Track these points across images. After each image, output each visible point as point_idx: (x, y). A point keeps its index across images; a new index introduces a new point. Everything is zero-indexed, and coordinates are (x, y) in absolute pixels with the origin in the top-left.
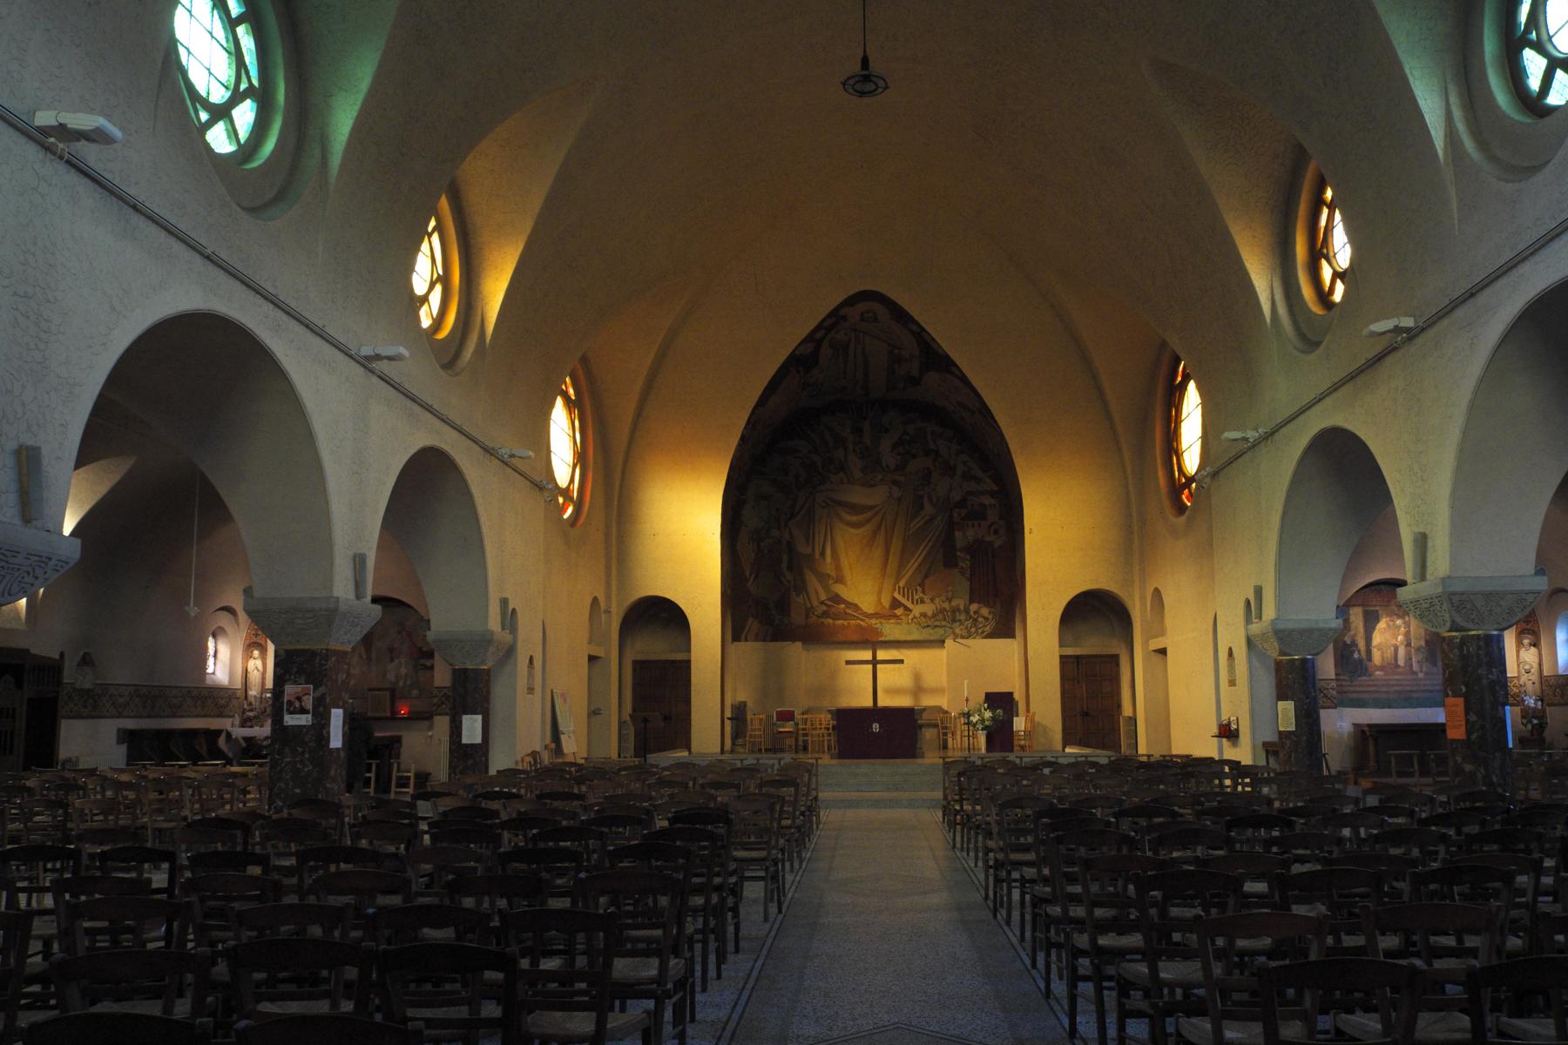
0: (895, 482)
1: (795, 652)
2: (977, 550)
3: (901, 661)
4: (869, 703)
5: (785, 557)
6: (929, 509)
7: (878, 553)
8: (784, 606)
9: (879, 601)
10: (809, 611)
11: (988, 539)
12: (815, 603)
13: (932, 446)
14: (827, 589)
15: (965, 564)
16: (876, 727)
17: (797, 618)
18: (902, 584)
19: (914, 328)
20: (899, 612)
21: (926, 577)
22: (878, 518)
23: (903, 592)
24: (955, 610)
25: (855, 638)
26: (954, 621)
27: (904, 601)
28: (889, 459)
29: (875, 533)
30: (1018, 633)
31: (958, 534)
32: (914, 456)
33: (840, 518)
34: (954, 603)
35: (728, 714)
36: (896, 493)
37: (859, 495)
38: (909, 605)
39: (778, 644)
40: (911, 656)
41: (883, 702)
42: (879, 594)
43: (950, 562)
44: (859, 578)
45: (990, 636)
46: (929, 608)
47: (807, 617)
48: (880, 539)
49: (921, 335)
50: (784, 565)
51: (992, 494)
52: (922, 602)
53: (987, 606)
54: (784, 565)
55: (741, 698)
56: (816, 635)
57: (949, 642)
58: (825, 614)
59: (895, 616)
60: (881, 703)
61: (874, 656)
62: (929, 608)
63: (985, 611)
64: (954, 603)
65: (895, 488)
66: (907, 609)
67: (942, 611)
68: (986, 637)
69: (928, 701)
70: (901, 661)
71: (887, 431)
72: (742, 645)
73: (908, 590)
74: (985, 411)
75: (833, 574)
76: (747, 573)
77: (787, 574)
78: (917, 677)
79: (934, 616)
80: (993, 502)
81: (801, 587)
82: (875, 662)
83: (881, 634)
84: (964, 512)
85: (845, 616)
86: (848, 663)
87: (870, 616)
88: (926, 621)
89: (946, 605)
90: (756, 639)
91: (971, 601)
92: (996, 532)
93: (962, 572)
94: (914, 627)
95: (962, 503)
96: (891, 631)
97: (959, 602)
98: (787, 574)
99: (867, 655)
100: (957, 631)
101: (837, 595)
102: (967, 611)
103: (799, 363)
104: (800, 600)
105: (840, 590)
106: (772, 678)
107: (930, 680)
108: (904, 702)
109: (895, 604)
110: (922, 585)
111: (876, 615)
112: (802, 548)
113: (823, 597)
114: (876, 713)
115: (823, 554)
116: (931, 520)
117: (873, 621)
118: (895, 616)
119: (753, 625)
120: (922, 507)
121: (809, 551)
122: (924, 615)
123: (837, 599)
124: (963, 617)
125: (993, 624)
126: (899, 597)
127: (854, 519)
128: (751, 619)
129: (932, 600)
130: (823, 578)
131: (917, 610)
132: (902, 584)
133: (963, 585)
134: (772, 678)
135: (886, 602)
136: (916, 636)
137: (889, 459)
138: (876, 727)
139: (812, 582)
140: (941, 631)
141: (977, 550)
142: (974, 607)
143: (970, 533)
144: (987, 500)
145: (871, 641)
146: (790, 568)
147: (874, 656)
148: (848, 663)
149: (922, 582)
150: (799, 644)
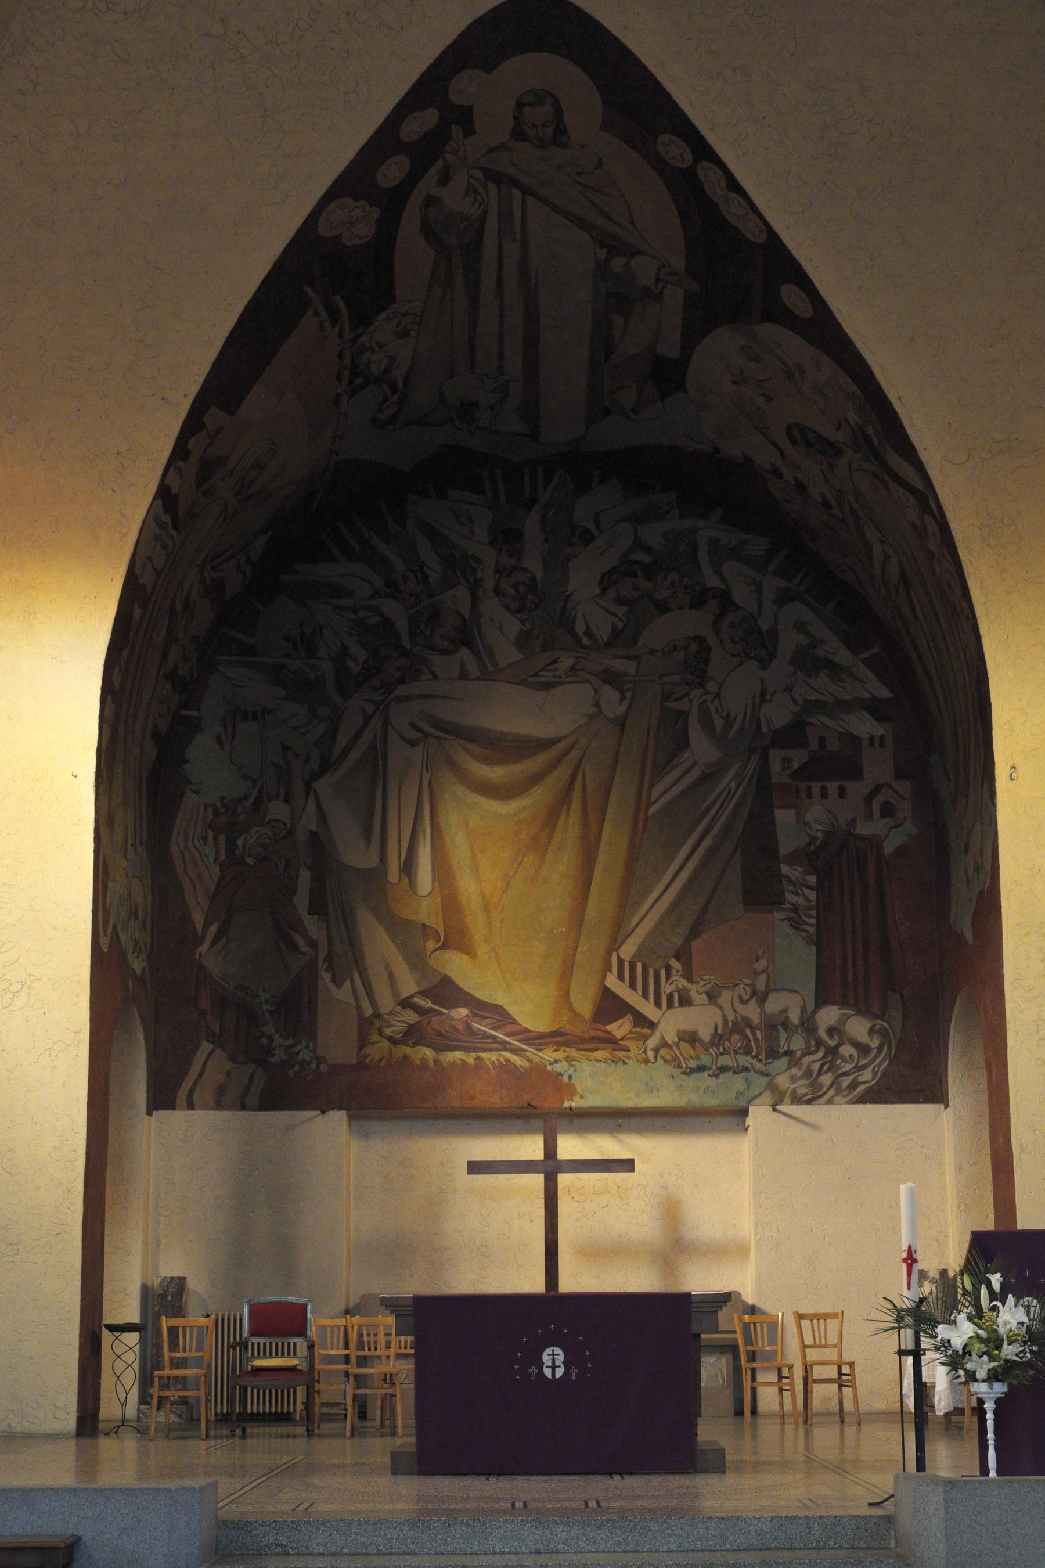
0: (610, 677)
1: (327, 1135)
2: (836, 859)
3: (627, 1165)
4: (534, 1283)
5: (305, 877)
6: (702, 749)
7: (561, 865)
8: (297, 1008)
9: (565, 998)
10: (367, 1026)
11: (863, 829)
12: (386, 1003)
13: (712, 581)
14: (418, 962)
15: (802, 890)
16: (553, 1361)
17: (335, 1043)
18: (628, 951)
19: (674, 150)
20: (619, 1028)
21: (695, 932)
22: (561, 774)
23: (628, 973)
24: (775, 1025)
25: (495, 1100)
26: (773, 1053)
27: (634, 999)
28: (594, 615)
29: (551, 818)
30: (961, 1078)
31: (783, 816)
32: (663, 608)
33: (452, 764)
34: (774, 1004)
35: (124, 1305)
36: (613, 704)
37: (513, 712)
38: (648, 1009)
39: (280, 1117)
40: (655, 1153)
41: (573, 1280)
42: (565, 977)
43: (762, 892)
44: (493, 883)
45: (874, 1096)
46: (701, 1019)
47: (363, 1043)
48: (570, 826)
49: (697, 185)
50: (301, 902)
51: (875, 709)
52: (685, 1001)
53: (863, 1009)
54: (301, 902)
55: (171, 1268)
56: (387, 1094)
57: (759, 1115)
58: (413, 1035)
59: (611, 1042)
60: (568, 1284)
61: (550, 1150)
62: (701, 1019)
63: (858, 1027)
64: (774, 1004)
65: (610, 693)
66: (641, 1020)
67: (740, 1026)
68: (864, 1099)
69: (700, 1280)
70: (627, 1165)
71: (587, 538)
72: (177, 1118)
73: (644, 971)
74: (882, 430)
75: (436, 922)
76: (198, 919)
77: (312, 926)
78: (672, 1212)
79: (717, 1039)
80: (878, 730)
81: (349, 960)
82: (551, 1167)
83: (570, 1090)
84: (798, 758)
85: (470, 1040)
86: (475, 1167)
87: (539, 1040)
88: (694, 1055)
89: (752, 1012)
90: (219, 1106)
91: (822, 999)
92: (887, 810)
93: (796, 924)
94: (661, 1071)
95: (792, 734)
96: (595, 1082)
97: (788, 1004)
98: (312, 926)
99: (532, 1148)
100: (783, 1081)
101: (447, 982)
102: (808, 1026)
103: (321, 281)
104: (343, 993)
105: (456, 966)
106: (262, 1210)
107: (706, 1221)
108: (637, 1279)
109: (610, 1006)
110: (683, 954)
111: (557, 1038)
112: (355, 854)
113: (409, 986)
114: (552, 1312)
115: (408, 867)
116: (708, 778)
117: (548, 1055)
118: (611, 1042)
119: (210, 1063)
120: (683, 742)
121: (369, 860)
122: (690, 1038)
123: (446, 992)
124: (798, 1043)
125: (882, 1062)
126: (622, 990)
127: (496, 773)
128: (206, 1047)
129: (712, 997)
130: (409, 935)
131: (671, 1024)
132: (628, 951)
133: (798, 958)
134: (262, 1210)
135: (584, 1003)
136: (666, 1097)
137: (594, 615)
138: (553, 1361)
139: (378, 944)
140: (738, 1082)
141: (836, 859)
142: (829, 1016)
143: (816, 813)
144: (863, 726)
145: (540, 1108)
146: (318, 906)
147: (550, 1150)
148: (475, 1167)
149: (683, 947)
150: (338, 1118)
